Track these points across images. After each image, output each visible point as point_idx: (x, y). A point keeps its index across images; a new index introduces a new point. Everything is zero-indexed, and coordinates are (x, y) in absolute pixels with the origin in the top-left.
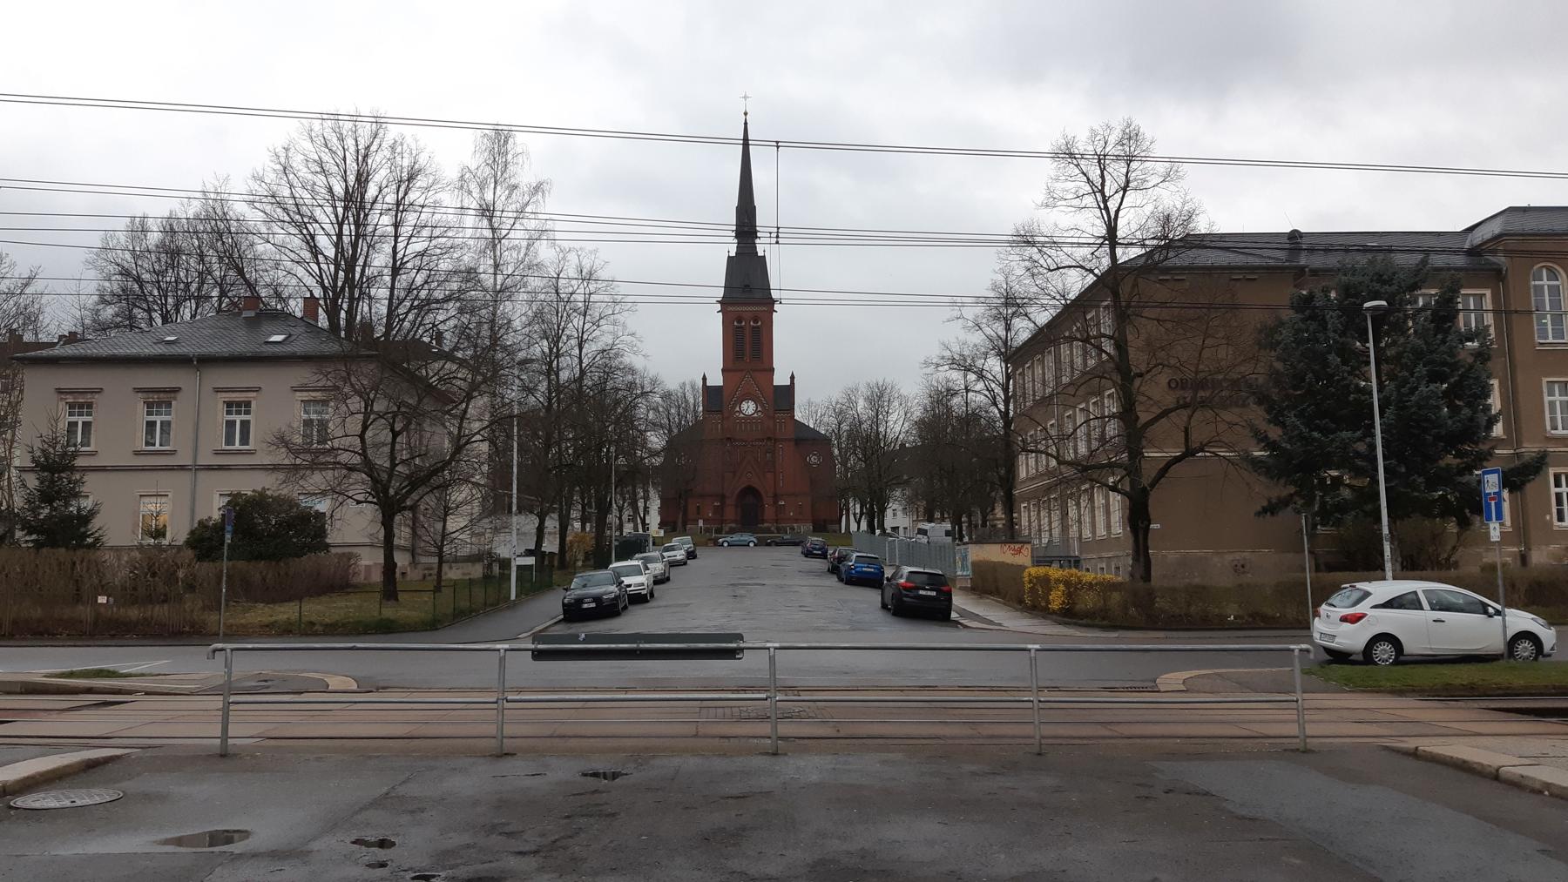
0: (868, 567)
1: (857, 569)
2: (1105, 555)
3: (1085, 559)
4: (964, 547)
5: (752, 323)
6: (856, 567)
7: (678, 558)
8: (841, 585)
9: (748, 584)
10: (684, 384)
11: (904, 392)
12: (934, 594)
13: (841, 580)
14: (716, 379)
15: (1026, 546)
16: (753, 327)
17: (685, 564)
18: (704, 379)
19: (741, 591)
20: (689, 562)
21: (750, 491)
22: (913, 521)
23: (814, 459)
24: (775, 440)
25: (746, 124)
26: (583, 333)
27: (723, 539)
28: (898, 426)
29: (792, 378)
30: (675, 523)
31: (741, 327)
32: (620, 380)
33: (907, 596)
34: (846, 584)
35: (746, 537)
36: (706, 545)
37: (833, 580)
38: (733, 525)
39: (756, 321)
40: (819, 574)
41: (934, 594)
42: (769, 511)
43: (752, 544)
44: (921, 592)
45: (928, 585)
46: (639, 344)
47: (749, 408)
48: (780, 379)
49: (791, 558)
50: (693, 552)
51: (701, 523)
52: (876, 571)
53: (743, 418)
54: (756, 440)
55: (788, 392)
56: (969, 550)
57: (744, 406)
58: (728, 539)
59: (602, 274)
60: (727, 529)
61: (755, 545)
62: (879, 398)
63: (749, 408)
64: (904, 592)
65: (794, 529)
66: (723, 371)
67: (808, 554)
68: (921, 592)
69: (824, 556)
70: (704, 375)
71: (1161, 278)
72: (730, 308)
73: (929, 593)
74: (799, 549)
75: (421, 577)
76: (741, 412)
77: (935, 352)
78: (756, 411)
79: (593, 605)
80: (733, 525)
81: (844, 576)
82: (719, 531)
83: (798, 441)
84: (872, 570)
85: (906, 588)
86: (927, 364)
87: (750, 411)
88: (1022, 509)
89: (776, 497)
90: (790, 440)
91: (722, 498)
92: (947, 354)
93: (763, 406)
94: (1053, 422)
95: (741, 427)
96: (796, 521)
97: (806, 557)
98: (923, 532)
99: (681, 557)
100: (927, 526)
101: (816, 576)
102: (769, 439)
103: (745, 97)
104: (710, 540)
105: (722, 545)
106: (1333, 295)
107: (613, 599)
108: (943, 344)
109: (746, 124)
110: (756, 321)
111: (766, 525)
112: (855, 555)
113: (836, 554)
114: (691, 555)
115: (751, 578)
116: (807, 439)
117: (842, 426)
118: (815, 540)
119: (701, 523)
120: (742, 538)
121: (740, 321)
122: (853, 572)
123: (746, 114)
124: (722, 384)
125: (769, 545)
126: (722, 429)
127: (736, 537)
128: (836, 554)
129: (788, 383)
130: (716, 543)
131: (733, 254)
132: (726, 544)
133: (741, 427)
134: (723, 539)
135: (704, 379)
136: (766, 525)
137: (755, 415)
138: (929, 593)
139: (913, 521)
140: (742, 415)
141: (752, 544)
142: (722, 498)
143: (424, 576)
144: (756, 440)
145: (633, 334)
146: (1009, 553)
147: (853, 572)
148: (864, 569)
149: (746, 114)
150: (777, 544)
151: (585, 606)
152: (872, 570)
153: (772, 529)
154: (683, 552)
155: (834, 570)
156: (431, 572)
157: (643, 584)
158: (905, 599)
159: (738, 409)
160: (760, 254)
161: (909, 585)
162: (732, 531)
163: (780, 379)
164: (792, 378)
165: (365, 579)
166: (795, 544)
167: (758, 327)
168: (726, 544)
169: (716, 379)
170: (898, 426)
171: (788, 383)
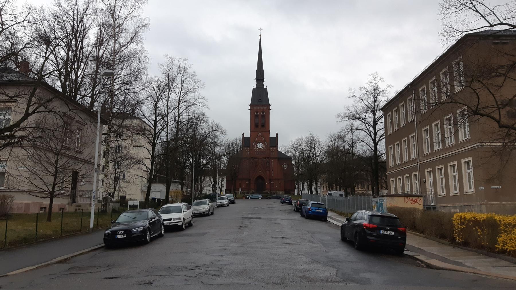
0: (319, 209)
1: (313, 211)
2: (457, 204)
3: (440, 207)
4: (380, 198)
5: (262, 114)
6: (312, 209)
7: (225, 203)
8: (303, 219)
9: (252, 218)
10: (236, 139)
11: (321, 140)
12: (393, 233)
13: (303, 216)
14: (248, 135)
15: (420, 198)
16: (262, 115)
17: (228, 206)
18: (243, 135)
19: (246, 223)
20: (230, 205)
21: (260, 178)
22: (322, 191)
23: (285, 166)
24: (270, 158)
25: (260, 39)
26: (180, 97)
27: (249, 196)
28: (320, 154)
29: (277, 134)
30: (231, 190)
31: (258, 115)
32: (203, 129)
33: (371, 235)
34: (306, 218)
35: (258, 195)
36: (242, 198)
37: (297, 216)
38: (254, 191)
39: (263, 113)
40: (289, 212)
41: (393, 233)
42: (267, 185)
43: (260, 198)
44: (383, 232)
45: (388, 226)
46: (206, 103)
47: (260, 146)
48: (272, 135)
49: (276, 204)
50: (233, 201)
51: (240, 190)
52: (323, 212)
53: (258, 150)
54: (263, 158)
55: (275, 140)
56: (385, 200)
57: (258, 145)
58: (251, 196)
59: (190, 71)
60: (251, 192)
61: (262, 199)
62: (312, 143)
63: (260, 146)
64: (368, 232)
65: (277, 193)
66: (250, 131)
67: (284, 202)
68: (383, 232)
69: (290, 203)
70: (243, 133)
71: (494, 41)
72: (253, 108)
73: (389, 233)
74: (280, 201)
75: (74, 210)
76: (257, 147)
77: (342, 111)
78: (263, 147)
79: (124, 236)
80: (254, 191)
81: (305, 214)
82: (248, 193)
83: (279, 159)
84: (321, 211)
85: (369, 229)
86: (339, 116)
87: (261, 147)
88: (391, 181)
89: (270, 180)
90: (276, 158)
91: (249, 180)
92: (347, 112)
93: (265, 145)
94: (414, 134)
95: (259, 153)
96: (278, 190)
97: (283, 203)
98: (331, 194)
99: (226, 203)
100: (331, 192)
101: (289, 213)
102: (268, 157)
103: (260, 30)
104: (244, 196)
105: (248, 199)
106: (373, 161)
107: (141, 232)
108: (346, 107)
109: (260, 39)
110: (263, 113)
111: (266, 191)
112: (311, 203)
113: (299, 202)
114: (232, 202)
115: (255, 214)
116: (283, 158)
117: (296, 153)
118: (285, 196)
119: (240, 190)
120: (256, 196)
121: (257, 113)
122: (311, 212)
123: (260, 36)
124: (249, 136)
125: (267, 198)
126: (250, 153)
127: (254, 195)
128: (299, 202)
129: (275, 136)
130: (246, 198)
131: (255, 88)
132: (250, 198)
133: (259, 153)
134: (249, 196)
135: (243, 135)
136: (266, 191)
137: (263, 148)
138: (389, 233)
139: (322, 191)
140: (257, 148)
141: (260, 198)
142: (249, 180)
143: (76, 210)
144: (263, 158)
145: (203, 98)
146: (409, 203)
147: (311, 212)
148: (317, 210)
149: (260, 36)
150: (270, 198)
151: (118, 237)
152: (321, 211)
153: (269, 193)
154: (227, 200)
155: (299, 209)
156: (80, 208)
157: (180, 219)
158: (368, 237)
159: (256, 146)
160: (265, 87)
161: (371, 225)
162: (252, 193)
163: (272, 135)
164: (277, 134)
165: (25, 211)
166: (278, 199)
167: (264, 115)
168: (250, 198)
169: (248, 135)
170: (320, 154)
171: (275, 136)
